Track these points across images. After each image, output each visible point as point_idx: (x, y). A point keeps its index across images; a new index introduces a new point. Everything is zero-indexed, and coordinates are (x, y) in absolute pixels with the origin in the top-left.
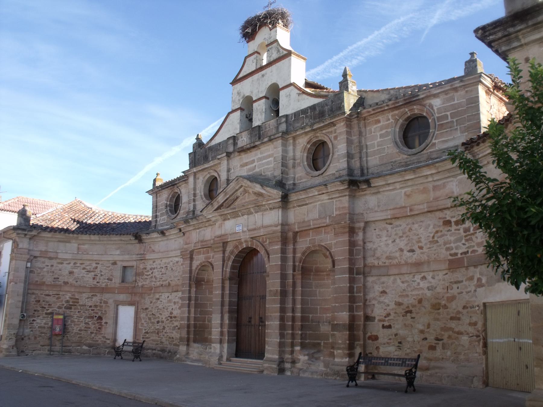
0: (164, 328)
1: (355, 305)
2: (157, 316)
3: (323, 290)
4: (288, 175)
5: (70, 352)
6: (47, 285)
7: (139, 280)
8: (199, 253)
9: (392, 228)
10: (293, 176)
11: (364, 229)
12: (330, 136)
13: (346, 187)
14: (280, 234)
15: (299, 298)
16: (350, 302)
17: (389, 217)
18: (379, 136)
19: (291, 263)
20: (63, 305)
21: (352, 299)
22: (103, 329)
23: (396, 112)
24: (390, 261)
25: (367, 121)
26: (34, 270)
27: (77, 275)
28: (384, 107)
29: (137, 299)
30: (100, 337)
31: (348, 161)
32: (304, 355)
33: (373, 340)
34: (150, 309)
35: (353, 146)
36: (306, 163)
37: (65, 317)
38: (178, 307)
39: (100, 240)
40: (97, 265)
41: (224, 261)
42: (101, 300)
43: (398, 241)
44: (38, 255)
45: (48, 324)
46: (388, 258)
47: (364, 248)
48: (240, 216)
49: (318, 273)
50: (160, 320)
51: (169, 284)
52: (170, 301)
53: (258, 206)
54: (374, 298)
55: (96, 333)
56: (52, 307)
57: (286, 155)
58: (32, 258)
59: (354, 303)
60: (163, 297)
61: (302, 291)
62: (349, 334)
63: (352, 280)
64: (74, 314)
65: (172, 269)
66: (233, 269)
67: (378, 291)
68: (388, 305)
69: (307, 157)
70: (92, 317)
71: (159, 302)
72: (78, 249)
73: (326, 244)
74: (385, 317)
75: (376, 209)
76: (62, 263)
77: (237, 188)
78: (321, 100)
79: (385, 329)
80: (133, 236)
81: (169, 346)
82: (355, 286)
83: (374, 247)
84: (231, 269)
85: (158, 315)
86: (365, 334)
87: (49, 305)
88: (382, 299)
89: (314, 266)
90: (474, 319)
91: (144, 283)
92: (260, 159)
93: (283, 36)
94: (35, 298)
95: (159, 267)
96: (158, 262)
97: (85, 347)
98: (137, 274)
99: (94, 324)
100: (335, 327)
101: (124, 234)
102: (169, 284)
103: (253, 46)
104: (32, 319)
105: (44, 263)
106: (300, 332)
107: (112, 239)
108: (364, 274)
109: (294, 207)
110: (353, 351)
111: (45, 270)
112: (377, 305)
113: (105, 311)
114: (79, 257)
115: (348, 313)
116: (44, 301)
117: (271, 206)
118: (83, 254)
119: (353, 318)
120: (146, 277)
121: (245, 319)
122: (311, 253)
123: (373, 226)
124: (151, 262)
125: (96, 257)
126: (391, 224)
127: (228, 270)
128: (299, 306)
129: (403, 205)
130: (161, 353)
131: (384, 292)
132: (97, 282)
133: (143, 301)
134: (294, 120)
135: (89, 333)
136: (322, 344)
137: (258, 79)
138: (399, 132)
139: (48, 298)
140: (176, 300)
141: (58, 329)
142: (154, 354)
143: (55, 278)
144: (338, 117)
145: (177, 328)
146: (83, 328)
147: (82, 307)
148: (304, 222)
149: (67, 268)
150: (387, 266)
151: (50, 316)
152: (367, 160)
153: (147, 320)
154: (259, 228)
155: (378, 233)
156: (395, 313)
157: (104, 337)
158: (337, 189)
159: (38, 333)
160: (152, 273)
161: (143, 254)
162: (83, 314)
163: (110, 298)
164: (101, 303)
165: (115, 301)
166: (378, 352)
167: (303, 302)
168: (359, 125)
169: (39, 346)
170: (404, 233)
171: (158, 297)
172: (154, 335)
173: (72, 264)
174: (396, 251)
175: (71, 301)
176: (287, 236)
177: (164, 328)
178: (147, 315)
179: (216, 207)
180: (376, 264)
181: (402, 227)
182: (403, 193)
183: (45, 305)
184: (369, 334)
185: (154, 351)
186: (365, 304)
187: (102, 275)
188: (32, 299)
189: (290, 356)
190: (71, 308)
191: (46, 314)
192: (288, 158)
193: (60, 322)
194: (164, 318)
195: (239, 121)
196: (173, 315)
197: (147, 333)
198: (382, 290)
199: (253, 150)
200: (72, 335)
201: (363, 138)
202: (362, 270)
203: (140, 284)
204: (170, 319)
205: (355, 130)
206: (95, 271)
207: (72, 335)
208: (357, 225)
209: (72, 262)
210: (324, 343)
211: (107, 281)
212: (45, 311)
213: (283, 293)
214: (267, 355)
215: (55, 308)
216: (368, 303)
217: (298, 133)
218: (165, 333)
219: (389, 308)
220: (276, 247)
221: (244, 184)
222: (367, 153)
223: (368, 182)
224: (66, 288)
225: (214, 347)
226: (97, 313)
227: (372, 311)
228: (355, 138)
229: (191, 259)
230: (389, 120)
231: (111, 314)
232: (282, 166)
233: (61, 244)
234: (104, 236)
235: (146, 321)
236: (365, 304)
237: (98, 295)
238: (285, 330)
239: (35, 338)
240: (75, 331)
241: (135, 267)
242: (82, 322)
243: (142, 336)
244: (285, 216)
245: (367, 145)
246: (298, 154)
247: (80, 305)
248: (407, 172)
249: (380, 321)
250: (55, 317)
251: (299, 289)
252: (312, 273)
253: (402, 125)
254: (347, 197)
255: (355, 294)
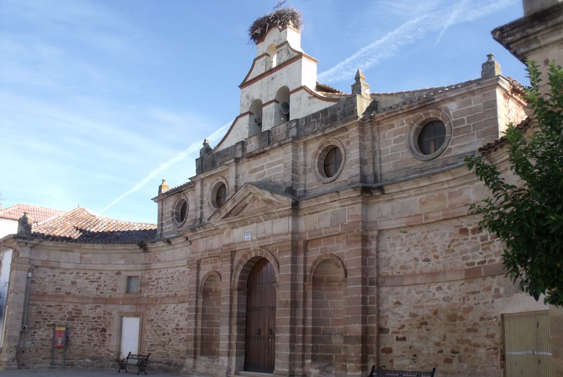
0: (170, 340)
1: (368, 317)
2: (163, 328)
3: (335, 301)
4: (298, 181)
5: (72, 365)
6: (49, 296)
7: (144, 291)
8: (206, 263)
9: (407, 237)
10: (303, 182)
11: (378, 238)
12: (342, 141)
13: (359, 194)
14: (290, 243)
15: (310, 309)
16: (363, 313)
17: (404, 225)
18: (393, 142)
19: (301, 273)
20: (66, 316)
21: (365, 310)
22: (107, 342)
23: (411, 116)
24: (405, 271)
25: (380, 126)
26: (36, 280)
27: (79, 286)
28: (398, 111)
29: (142, 310)
30: (104, 349)
31: (360, 167)
32: (316, 369)
33: (386, 353)
34: (156, 320)
35: (366, 152)
36: (317, 169)
37: (67, 329)
38: (184, 318)
39: (103, 249)
40: (100, 275)
41: (232, 271)
42: (105, 311)
43: (412, 250)
44: (40, 265)
45: (50, 336)
46: (403, 267)
47: (377, 257)
48: (248, 224)
49: (330, 284)
50: (166, 332)
51: (176, 295)
52: (176, 312)
53: (267, 214)
54: (388, 310)
55: (100, 346)
56: (54, 319)
57: (296, 160)
58: (34, 268)
59: (367, 314)
60: (169, 308)
61: (313, 302)
62: (362, 346)
63: (365, 291)
64: (77, 325)
65: (178, 279)
66: (242, 280)
67: (392, 301)
68: (403, 317)
69: (319, 163)
70: (96, 329)
71: (165, 313)
72: (81, 258)
73: (338, 253)
74: (399, 329)
75: (390, 217)
76: (64, 273)
77: (246, 195)
78: (332, 104)
79: (399, 342)
80: (138, 244)
81: (175, 359)
82: (368, 297)
83: (388, 256)
84: (239, 279)
85: (163, 327)
86: (378, 346)
87: (51, 316)
88: (396, 310)
89: (326, 276)
90: (491, 331)
91: (150, 294)
92: (269, 165)
93: (294, 37)
94: (36, 310)
95: (165, 277)
96: (164, 271)
97: (88, 360)
98: (142, 285)
99: (98, 336)
100: (347, 339)
101: (128, 243)
102: (176, 295)
103: (263, 47)
104: (33, 331)
105: (45, 272)
106: (311, 345)
107: (116, 248)
108: (377, 284)
109: (305, 215)
110: (365, 364)
111: (46, 280)
112: (390, 317)
113: (109, 323)
114: (82, 266)
115: (361, 325)
116: (45, 312)
117: (281, 214)
118: (85, 263)
119: (365, 330)
120: (151, 287)
121: (254, 331)
122: (322, 262)
123: (387, 234)
124: (157, 272)
125: (99, 267)
126: (405, 232)
127: (237, 280)
128: (310, 318)
129: (418, 213)
130: (167, 366)
131: (398, 303)
132: (101, 293)
133: (148, 312)
134: (305, 124)
135: (92, 344)
136: (334, 357)
137: (268, 82)
138: (414, 137)
139: (50, 310)
140: (183, 312)
141: (60, 341)
142: (160, 367)
143: (57, 289)
144: (350, 121)
145: (183, 340)
146: (86, 341)
147: (85, 319)
148: (315, 230)
149: (69, 278)
150: (402, 276)
151: (51, 328)
152: (380, 166)
153: (153, 332)
154: (269, 237)
155: (392, 242)
156: (410, 325)
157: (108, 350)
158: (349, 196)
159: (39, 345)
160: (158, 283)
161: (148, 264)
162: (87, 326)
163: (114, 309)
164: (104, 314)
165: (120, 313)
166: (392, 365)
167: (314, 313)
168: (372, 130)
169: (41, 359)
170: (418, 242)
171: (163, 308)
172: (160, 347)
173: (74, 274)
174: (411, 261)
175: (74, 312)
176: (298, 245)
177: (170, 340)
178: (152, 327)
179: (224, 215)
180: (390, 274)
181: (417, 236)
182: (418, 200)
183: (46, 316)
184: (382, 347)
185: (160, 365)
186: (378, 315)
187: (105, 285)
188: (33, 310)
189: (301, 370)
190: (73, 320)
191: (48, 325)
192: (298, 165)
193: (63, 334)
194: (170, 329)
195: (248, 125)
196: (179, 327)
197: (152, 345)
198: (396, 301)
199: (262, 155)
200: (75, 347)
201: (376, 143)
202: (376, 280)
203: (145, 295)
204: (176, 331)
205: (369, 134)
206: (98, 282)
207: (75, 347)
208: (370, 233)
209: (75, 272)
210: (336, 356)
211: (111, 291)
212: (47, 323)
213: (294, 304)
214: (277, 369)
215: (57, 319)
216: (381, 314)
217: (309, 138)
218: (171, 345)
219: (403, 319)
220: (286, 257)
221: (253, 191)
222: (380, 158)
223: (381, 189)
224: (69, 299)
225: (222, 360)
226: (101, 325)
227: (386, 323)
228: (368, 143)
229: (198, 268)
230: (403, 124)
231: (115, 326)
232: (293, 172)
233: (64, 254)
234: (107, 245)
235: (151, 333)
236: (378, 315)
237: (102, 306)
238: (295, 342)
239: (37, 350)
240: (77, 343)
241: (140, 277)
242: (85, 334)
243: (147, 349)
244: (295, 224)
245: (380, 151)
246: (309, 160)
247: (83, 317)
248: (422, 179)
249: (394, 333)
250: (57, 329)
251: (310, 300)
252: (324, 284)
253: (417, 130)
254: (360, 205)
255: (368, 305)
